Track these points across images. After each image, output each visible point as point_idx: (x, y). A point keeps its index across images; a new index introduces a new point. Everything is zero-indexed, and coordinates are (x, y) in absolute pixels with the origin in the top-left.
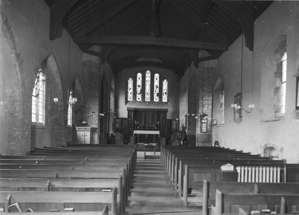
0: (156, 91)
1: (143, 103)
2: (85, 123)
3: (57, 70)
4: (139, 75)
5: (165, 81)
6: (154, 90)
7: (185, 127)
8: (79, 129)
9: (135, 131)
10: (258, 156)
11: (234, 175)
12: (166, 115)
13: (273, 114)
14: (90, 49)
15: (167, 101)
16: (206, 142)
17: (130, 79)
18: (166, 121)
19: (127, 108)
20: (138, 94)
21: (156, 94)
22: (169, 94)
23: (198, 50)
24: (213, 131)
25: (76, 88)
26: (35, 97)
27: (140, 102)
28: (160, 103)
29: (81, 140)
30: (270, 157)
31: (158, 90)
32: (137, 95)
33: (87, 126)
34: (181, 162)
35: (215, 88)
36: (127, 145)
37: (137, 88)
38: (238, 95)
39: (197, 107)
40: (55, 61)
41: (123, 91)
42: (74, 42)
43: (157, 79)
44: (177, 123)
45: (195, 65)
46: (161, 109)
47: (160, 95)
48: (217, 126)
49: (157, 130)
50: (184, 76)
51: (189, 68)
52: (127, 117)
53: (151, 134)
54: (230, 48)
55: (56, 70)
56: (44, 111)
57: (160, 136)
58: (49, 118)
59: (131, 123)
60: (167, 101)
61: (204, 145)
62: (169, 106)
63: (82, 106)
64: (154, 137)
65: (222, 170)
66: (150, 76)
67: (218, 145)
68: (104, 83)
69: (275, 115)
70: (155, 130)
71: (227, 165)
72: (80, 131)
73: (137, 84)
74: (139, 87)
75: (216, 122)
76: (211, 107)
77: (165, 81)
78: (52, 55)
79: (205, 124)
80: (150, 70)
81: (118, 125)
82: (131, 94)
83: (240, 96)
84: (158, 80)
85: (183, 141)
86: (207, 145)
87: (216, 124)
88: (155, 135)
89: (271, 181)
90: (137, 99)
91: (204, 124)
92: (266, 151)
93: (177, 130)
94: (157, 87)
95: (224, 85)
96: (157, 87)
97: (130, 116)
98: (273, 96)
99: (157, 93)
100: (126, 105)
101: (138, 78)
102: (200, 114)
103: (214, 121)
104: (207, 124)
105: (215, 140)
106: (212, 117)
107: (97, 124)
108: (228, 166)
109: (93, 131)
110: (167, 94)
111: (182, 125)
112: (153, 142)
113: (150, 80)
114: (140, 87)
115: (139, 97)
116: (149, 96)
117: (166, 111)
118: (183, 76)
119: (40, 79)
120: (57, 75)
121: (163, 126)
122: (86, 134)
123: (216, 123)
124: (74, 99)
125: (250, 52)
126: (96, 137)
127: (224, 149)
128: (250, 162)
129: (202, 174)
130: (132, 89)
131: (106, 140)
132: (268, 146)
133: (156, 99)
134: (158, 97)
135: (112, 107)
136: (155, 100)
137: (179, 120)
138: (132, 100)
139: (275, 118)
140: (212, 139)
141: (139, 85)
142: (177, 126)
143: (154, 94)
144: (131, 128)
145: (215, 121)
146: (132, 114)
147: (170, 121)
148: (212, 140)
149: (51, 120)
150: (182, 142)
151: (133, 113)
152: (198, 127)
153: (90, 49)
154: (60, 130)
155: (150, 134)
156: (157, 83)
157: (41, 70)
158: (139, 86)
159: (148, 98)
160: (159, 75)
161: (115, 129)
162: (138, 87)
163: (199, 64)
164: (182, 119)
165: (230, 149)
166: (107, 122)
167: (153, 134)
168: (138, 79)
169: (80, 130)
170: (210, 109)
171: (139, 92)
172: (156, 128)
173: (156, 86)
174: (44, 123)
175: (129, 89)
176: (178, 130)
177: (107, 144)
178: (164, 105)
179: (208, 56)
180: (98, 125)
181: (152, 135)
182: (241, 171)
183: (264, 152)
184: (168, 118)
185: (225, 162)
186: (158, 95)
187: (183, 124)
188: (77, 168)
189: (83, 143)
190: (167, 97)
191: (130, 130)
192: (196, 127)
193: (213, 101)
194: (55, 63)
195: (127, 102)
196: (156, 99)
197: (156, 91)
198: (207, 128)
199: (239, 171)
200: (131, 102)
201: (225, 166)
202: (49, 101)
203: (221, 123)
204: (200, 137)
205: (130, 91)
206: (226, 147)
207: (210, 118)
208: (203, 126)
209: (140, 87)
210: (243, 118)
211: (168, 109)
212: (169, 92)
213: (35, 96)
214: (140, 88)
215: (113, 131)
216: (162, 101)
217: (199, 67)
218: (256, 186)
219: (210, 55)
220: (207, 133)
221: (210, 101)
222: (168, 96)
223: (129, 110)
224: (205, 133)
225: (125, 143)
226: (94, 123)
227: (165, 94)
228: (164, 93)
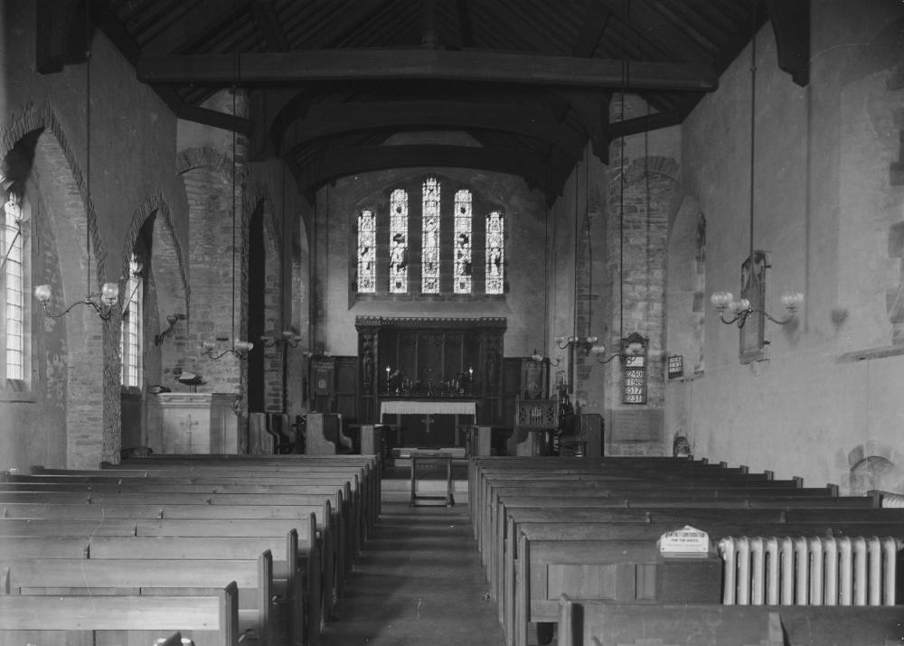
0: (463, 253)
1: (414, 301)
4: (399, 197)
5: (495, 215)
8: (171, 399)
9: (387, 403)
10: (828, 493)
11: (709, 574)
12: (499, 342)
13: (889, 327)
14: (205, 105)
15: (502, 292)
16: (640, 441)
17: (367, 213)
19: (358, 320)
20: (395, 268)
21: (461, 266)
22: (509, 265)
23: (608, 91)
25: (155, 252)
28: (476, 299)
29: (177, 441)
30: (872, 495)
31: (470, 251)
33: (199, 388)
36: (304, 456)
37: (393, 244)
40: (61, 150)
42: (141, 80)
43: (463, 211)
44: (542, 372)
46: (481, 319)
47: (476, 269)
48: (682, 381)
52: (355, 354)
53: (416, 412)
54: (724, 78)
55: (68, 184)
56: (29, 335)
58: (48, 362)
59: (370, 376)
60: (502, 292)
61: (633, 450)
62: (511, 307)
63: (182, 317)
66: (438, 199)
67: (687, 450)
68: (265, 230)
69: (896, 334)
71: (684, 531)
72: (174, 407)
73: (392, 230)
74: (399, 242)
76: (657, 307)
77: (495, 215)
78: (48, 130)
81: (322, 384)
82: (368, 268)
83: (762, 263)
84: (469, 213)
86: (644, 451)
87: (680, 374)
88: (461, 416)
89: (847, 601)
90: (393, 285)
91: (632, 374)
92: (859, 472)
93: (540, 398)
94: (466, 241)
95: (705, 221)
96: (466, 241)
97: (368, 348)
98: (886, 256)
99: (466, 262)
101: (395, 208)
103: (671, 360)
105: (675, 432)
107: (235, 380)
108: (687, 534)
109: (219, 401)
110: (502, 267)
111: (560, 379)
112: (451, 445)
115: (398, 276)
116: (438, 275)
117: (499, 328)
118: (559, 197)
122: (193, 421)
123: (677, 370)
124: (109, 287)
125: (798, 92)
126: (232, 427)
129: (586, 568)
131: (272, 437)
132: (866, 455)
133: (462, 285)
135: (301, 316)
136: (457, 290)
137: (547, 361)
138: (374, 290)
139: (895, 342)
141: (399, 235)
142: (539, 382)
143: (456, 265)
144: (371, 393)
146: (376, 343)
147: (517, 363)
149: (56, 368)
151: (376, 336)
152: (611, 384)
153: (205, 105)
154: (91, 403)
156: (463, 225)
158: (398, 238)
159: (431, 279)
161: (313, 398)
162: (396, 243)
163: (613, 148)
164: (559, 354)
167: (454, 415)
168: (393, 213)
170: (656, 316)
171: (401, 260)
173: (462, 236)
174: (29, 380)
175: (360, 251)
176: (543, 396)
177: (276, 453)
178: (491, 308)
179: (644, 114)
180: (238, 384)
181: (450, 417)
182: (737, 554)
183: (853, 479)
184: (505, 356)
185: (676, 520)
186: (468, 269)
188: (101, 550)
189: (184, 451)
190: (502, 277)
193: (665, 283)
194: (65, 160)
195: (354, 297)
196: (462, 285)
197: (463, 253)
198: (644, 386)
199: (729, 556)
200: (369, 299)
203: (699, 370)
205: (367, 259)
206: (714, 461)
207: (657, 349)
208: (629, 382)
209: (403, 241)
211: (505, 321)
212: (508, 257)
214: (402, 245)
215: (304, 405)
216: (484, 291)
217: (612, 160)
218: (774, 618)
219: (654, 111)
220: (645, 407)
221: (656, 284)
222: (505, 274)
223: (363, 328)
224: (637, 407)
225: (341, 449)
226: (227, 376)
227: (494, 266)
228: (493, 261)
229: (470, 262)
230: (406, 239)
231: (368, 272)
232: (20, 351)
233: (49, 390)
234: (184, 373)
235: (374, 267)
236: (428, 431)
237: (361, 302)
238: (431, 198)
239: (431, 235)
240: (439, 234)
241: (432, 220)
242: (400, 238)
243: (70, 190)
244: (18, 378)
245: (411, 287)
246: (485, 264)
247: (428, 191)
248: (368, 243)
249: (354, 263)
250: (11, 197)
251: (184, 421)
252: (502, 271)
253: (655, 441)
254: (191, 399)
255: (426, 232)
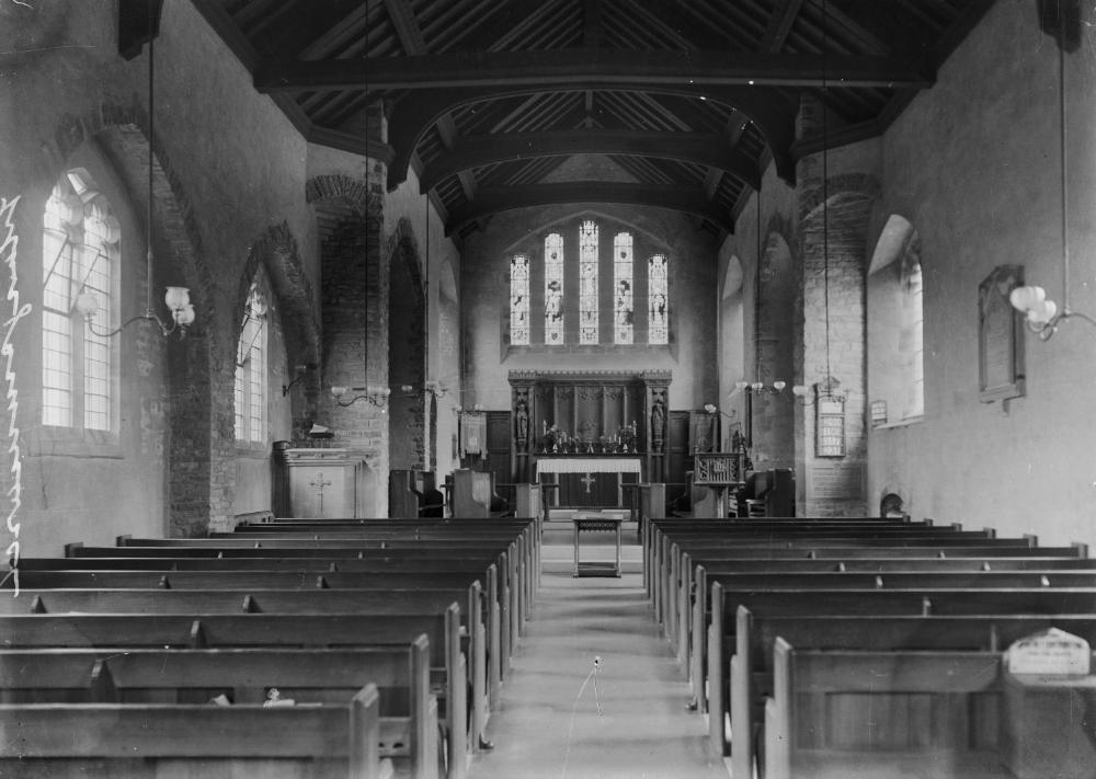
0: (624, 301)
2: (323, 430)
3: (170, 199)
5: (658, 259)
6: (616, 300)
7: (744, 439)
15: (666, 342)
17: (520, 260)
18: (665, 418)
24: (870, 452)
26: (65, 319)
27: (558, 349)
29: (307, 504)
31: (632, 299)
32: (549, 322)
34: (742, 611)
35: (873, 268)
37: (548, 292)
38: (995, 276)
39: (796, 349)
41: (490, 309)
43: (624, 255)
45: (781, 174)
47: (638, 317)
49: (630, 455)
50: (733, 233)
51: (754, 196)
52: (509, 408)
56: (118, 379)
57: (645, 480)
64: (620, 482)
65: (1012, 671)
66: (596, 243)
67: (897, 509)
70: (621, 455)
72: (304, 465)
74: (554, 290)
75: (882, 411)
77: (658, 259)
79: (838, 422)
80: (598, 221)
82: (522, 319)
84: (630, 257)
85: (738, 498)
86: (850, 514)
90: (548, 336)
91: (828, 422)
94: (627, 287)
97: (522, 402)
99: (628, 311)
100: (506, 363)
102: (812, 379)
104: (843, 419)
105: (884, 487)
106: (865, 392)
110: (666, 315)
111: (734, 433)
113: (597, 260)
114: (559, 288)
115: (554, 329)
116: (597, 325)
119: (253, 314)
120: (171, 221)
121: (654, 437)
123: (883, 416)
127: (909, 523)
128: (992, 569)
130: (528, 299)
133: (624, 335)
134: (631, 326)
137: (718, 414)
138: (528, 343)
140: (866, 483)
141: (554, 283)
143: (616, 314)
145: (881, 405)
148: (866, 489)
150: (736, 502)
155: (604, 474)
156: (623, 270)
157: (94, 198)
160: (631, 238)
161: (463, 456)
162: (551, 291)
163: (800, 166)
165: (965, 529)
166: (423, 426)
169: (303, 459)
171: (557, 309)
172: (626, 447)
173: (623, 283)
174: (117, 431)
187: (734, 429)
189: (316, 515)
190: (666, 325)
191: (523, 459)
192: (796, 435)
196: (624, 335)
197: (624, 301)
200: (522, 352)
201: (1032, 648)
202: (143, 339)
204: (815, 479)
205: (520, 309)
210: (1029, 383)
213: (65, 310)
214: (557, 293)
222: (670, 323)
223: (516, 381)
227: (657, 314)
228: (657, 309)
229: (631, 310)
230: (562, 287)
231: (521, 322)
232: (107, 397)
233: (144, 444)
234: (315, 426)
235: (528, 317)
236: (588, 490)
237: (515, 356)
238: (589, 242)
239: (589, 282)
240: (597, 281)
241: (589, 266)
242: (555, 286)
243: (169, 208)
244: (103, 428)
245: (567, 338)
246: (648, 311)
247: (585, 235)
248: (521, 292)
249: (506, 315)
250: (94, 212)
251: (315, 481)
252: (666, 320)
253: (857, 499)
254: (323, 456)
255: (583, 279)
